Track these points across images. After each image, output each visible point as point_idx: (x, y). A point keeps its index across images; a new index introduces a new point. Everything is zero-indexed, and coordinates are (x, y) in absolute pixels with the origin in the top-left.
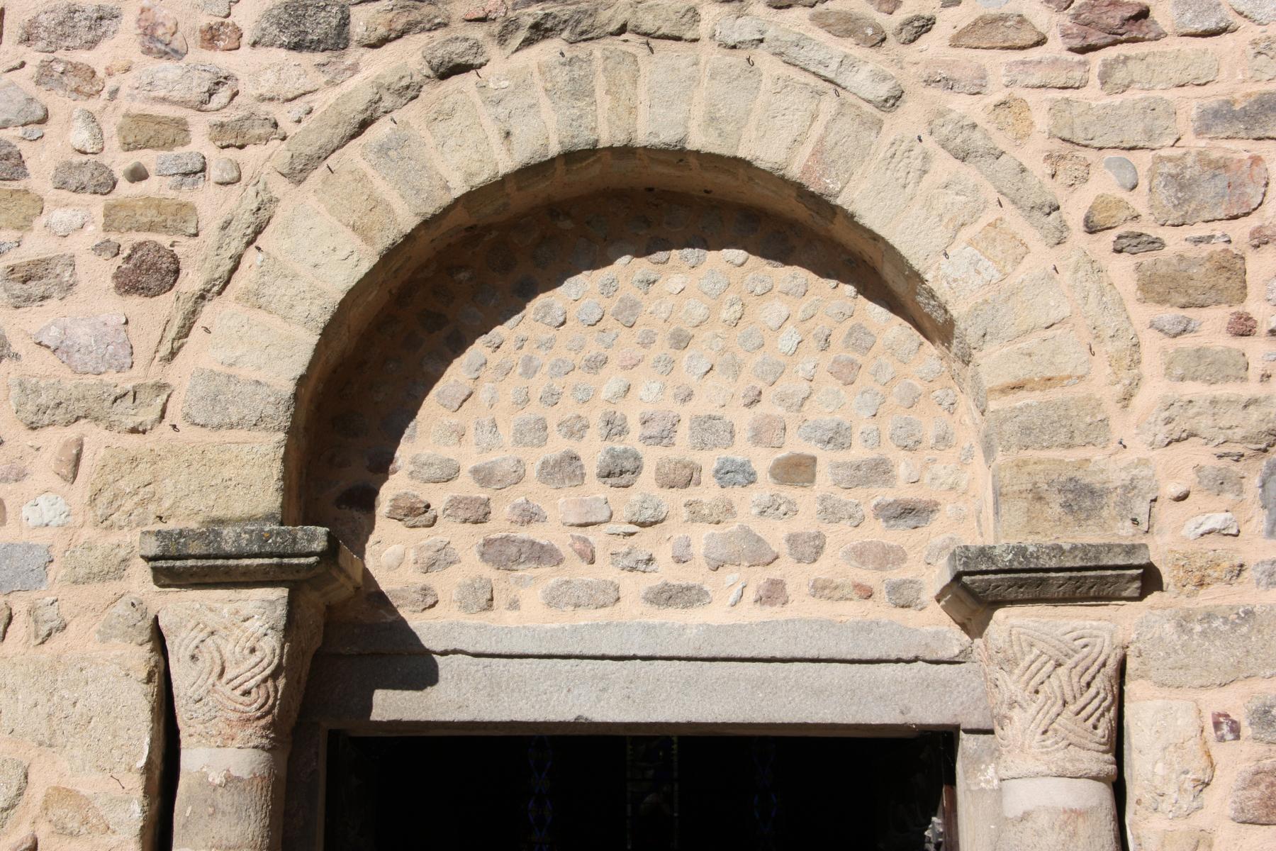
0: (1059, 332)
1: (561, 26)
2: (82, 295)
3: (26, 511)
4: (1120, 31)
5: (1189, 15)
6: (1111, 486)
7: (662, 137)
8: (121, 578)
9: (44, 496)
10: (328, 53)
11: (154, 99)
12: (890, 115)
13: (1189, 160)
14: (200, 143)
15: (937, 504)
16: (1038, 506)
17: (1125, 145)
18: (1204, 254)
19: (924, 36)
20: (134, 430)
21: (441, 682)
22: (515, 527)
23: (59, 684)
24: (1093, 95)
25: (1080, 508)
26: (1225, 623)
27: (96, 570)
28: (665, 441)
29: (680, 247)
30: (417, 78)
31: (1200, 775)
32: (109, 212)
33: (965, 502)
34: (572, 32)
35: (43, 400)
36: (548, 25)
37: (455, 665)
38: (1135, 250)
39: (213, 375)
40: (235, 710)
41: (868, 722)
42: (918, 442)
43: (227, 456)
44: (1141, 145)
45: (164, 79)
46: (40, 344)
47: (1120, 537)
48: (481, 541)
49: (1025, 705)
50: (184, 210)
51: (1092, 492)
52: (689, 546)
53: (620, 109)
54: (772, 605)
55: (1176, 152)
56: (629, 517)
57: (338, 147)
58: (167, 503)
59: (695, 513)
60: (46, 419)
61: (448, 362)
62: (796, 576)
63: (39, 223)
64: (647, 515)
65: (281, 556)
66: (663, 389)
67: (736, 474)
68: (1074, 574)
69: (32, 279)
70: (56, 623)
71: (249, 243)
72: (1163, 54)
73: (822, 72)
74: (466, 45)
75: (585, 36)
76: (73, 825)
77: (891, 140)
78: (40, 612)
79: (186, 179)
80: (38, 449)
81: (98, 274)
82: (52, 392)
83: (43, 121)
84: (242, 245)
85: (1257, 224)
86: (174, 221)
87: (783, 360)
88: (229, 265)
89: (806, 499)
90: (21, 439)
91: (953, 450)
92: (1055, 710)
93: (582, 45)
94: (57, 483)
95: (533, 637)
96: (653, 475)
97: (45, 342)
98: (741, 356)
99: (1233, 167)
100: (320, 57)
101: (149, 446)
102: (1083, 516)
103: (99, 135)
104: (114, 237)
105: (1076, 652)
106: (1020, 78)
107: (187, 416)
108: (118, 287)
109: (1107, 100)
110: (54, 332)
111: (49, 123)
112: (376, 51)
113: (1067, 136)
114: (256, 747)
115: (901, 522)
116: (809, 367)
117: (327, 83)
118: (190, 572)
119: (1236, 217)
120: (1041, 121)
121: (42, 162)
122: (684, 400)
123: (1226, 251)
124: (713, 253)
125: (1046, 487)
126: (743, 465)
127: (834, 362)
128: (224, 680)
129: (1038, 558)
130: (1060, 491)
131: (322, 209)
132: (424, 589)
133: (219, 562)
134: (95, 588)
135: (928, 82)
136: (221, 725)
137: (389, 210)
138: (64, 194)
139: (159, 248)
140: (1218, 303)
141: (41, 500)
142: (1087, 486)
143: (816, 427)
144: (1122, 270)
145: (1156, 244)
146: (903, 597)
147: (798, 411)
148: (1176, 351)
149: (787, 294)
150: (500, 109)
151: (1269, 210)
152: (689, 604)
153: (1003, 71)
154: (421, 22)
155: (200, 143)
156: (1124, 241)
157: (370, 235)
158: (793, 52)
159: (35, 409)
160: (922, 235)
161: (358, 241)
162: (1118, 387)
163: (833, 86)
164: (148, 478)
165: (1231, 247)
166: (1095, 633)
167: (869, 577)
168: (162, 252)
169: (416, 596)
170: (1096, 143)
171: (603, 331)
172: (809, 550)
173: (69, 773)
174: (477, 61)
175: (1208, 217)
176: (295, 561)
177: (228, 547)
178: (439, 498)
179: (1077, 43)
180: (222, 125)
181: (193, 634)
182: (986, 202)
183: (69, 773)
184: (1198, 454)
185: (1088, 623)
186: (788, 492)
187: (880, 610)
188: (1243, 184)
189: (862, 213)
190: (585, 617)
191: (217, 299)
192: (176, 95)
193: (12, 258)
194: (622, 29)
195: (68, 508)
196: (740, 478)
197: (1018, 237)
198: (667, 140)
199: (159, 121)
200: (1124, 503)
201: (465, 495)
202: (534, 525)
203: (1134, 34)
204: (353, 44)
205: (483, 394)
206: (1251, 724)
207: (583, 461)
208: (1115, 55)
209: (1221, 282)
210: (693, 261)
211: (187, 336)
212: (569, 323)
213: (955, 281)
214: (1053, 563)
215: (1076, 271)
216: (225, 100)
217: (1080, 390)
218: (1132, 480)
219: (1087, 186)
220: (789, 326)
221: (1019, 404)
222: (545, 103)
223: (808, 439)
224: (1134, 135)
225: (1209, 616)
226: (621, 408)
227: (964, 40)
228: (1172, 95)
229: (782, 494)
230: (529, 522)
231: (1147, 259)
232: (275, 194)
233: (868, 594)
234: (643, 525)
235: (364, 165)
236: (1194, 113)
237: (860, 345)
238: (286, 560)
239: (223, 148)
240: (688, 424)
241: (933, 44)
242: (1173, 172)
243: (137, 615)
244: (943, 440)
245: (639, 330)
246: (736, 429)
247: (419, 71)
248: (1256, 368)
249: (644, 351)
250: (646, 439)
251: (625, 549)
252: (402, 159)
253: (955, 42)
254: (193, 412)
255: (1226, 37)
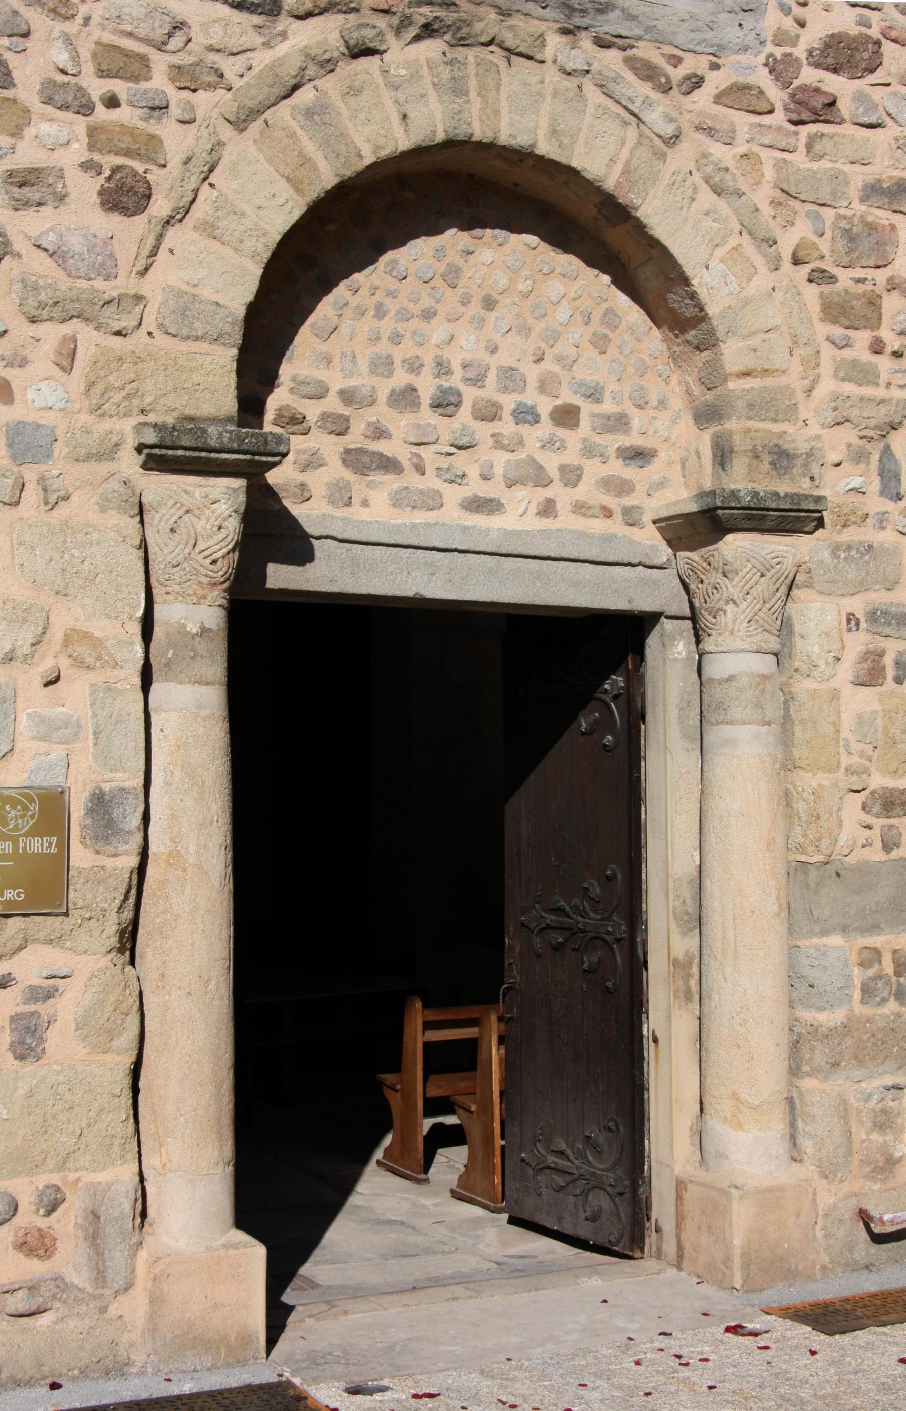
0: (773, 336)
1: (445, 30)
2: (73, 207)
3: (31, 395)
4: (821, 113)
5: (861, 110)
6: (799, 452)
7: (519, 140)
8: (113, 459)
9: (47, 382)
10: (263, 17)
11: (122, 32)
12: (671, 150)
13: (856, 220)
14: (159, 80)
15: (656, 451)
16: (755, 462)
17: (819, 202)
18: (860, 291)
19: (696, 91)
20: (118, 333)
21: (316, 561)
22: (367, 441)
23: (69, 544)
24: (799, 159)
25: (781, 467)
26: (857, 553)
27: (94, 451)
28: (479, 383)
29: (493, 227)
30: (336, 54)
31: (837, 654)
32: (92, 132)
33: (674, 451)
34: (453, 36)
35: (43, 297)
36: (435, 27)
37: (326, 547)
38: (820, 281)
39: (181, 293)
40: (206, 575)
41: (608, 607)
42: (647, 403)
43: (194, 364)
44: (829, 203)
45: (129, 14)
46: (39, 246)
47: (803, 489)
48: (342, 450)
49: (739, 602)
50: (154, 141)
51: (788, 456)
52: (492, 467)
53: (488, 111)
54: (547, 517)
55: (849, 213)
56: (452, 441)
57: (274, 105)
58: (149, 399)
59: (498, 443)
60: (45, 314)
61: (319, 300)
62: (563, 496)
63: (29, 133)
64: (465, 441)
65: (253, 454)
66: (477, 342)
67: (526, 415)
68: (783, 513)
69: (30, 185)
70: (62, 493)
71: (205, 179)
72: (844, 136)
73: (630, 106)
74: (375, 31)
75: (462, 42)
76: (89, 660)
77: (673, 170)
78: (48, 483)
79: (153, 113)
80: (38, 341)
81: (85, 189)
82: (50, 292)
83: (26, 35)
84: (199, 181)
85: (891, 274)
86: (147, 150)
87: (559, 328)
88: (190, 197)
89: (573, 438)
90: (21, 330)
91: (667, 412)
92: (758, 607)
93: (460, 49)
94: (56, 372)
95: (384, 529)
96: (470, 410)
97: (45, 245)
98: (531, 321)
99: (879, 229)
100: (257, 19)
101: (130, 348)
102: (782, 472)
103: (75, 58)
104: (96, 157)
105: (772, 567)
106: (758, 137)
107: (161, 326)
108: (102, 204)
109: (809, 165)
110: (52, 237)
111: (31, 37)
112: (301, 22)
113: (786, 189)
114: (220, 606)
115: (632, 462)
116: (577, 336)
117: (264, 44)
118: (176, 459)
119: (879, 267)
120: (769, 173)
121: (29, 72)
122: (492, 352)
123: (873, 290)
124: (515, 235)
125: (761, 449)
126: (532, 408)
127: (594, 335)
128: (197, 550)
129: (765, 500)
130: (769, 453)
131: (261, 157)
132: (302, 485)
133: (203, 454)
134: (92, 466)
135: (698, 128)
136: (195, 587)
137: (315, 168)
138: (50, 109)
139: (136, 174)
140: (865, 328)
141: (43, 385)
142: (785, 450)
143: (582, 384)
144: (812, 293)
145: (832, 279)
146: (631, 517)
147: (570, 370)
148: (842, 359)
149: (564, 276)
150: (399, 94)
151: (897, 264)
152: (490, 512)
153: (746, 129)
154: (338, 4)
155: (159, 80)
156: (815, 274)
157: (301, 187)
158: (611, 86)
159: (36, 304)
160: (692, 250)
161: (292, 192)
162: (807, 381)
163: (636, 120)
164: (132, 376)
165: (876, 288)
166: (785, 554)
167: (611, 502)
168: (138, 178)
169: (297, 491)
170: (802, 197)
171: (433, 288)
172: (573, 478)
173: (82, 618)
174: (382, 48)
175: (864, 264)
176: (264, 459)
177: (213, 443)
178: (312, 411)
179: (795, 117)
180: (179, 68)
181: (172, 511)
182: (732, 230)
183: (82, 618)
184: (848, 435)
185: (781, 548)
186: (562, 432)
187: (616, 526)
188: (885, 244)
189: (653, 225)
190: (421, 517)
191: (178, 225)
192: (142, 32)
193: (9, 164)
194: (490, 43)
195: (67, 395)
196: (529, 418)
197: (751, 261)
198: (522, 143)
199: (127, 54)
200: (806, 465)
201: (333, 411)
202: (382, 441)
203: (829, 117)
204: (284, 12)
205: (345, 329)
206: (866, 621)
207: (420, 393)
208: (815, 131)
209: (869, 313)
210: (501, 240)
211: (155, 255)
212: (409, 279)
213: (712, 288)
214: (774, 505)
215: (786, 293)
216: (181, 45)
217: (782, 380)
218: (811, 449)
219: (794, 228)
220: (564, 302)
221: (747, 386)
222: (433, 95)
223: (576, 393)
224: (825, 197)
225: (849, 548)
226: (446, 354)
227: (723, 100)
228: (847, 168)
229: (558, 434)
230: (379, 438)
231: (827, 289)
232: (223, 138)
233: (608, 513)
234: (460, 448)
235: (293, 124)
236: (860, 185)
237: (611, 324)
238: (257, 458)
239: (180, 88)
240: (495, 372)
241: (702, 99)
242: (847, 227)
243: (129, 492)
244: (662, 403)
245: (459, 291)
246: (528, 380)
247: (338, 48)
248: (884, 377)
249: (463, 309)
250: (466, 380)
251: (445, 466)
252: (324, 124)
253: (718, 99)
254: (167, 323)
255: (879, 130)
